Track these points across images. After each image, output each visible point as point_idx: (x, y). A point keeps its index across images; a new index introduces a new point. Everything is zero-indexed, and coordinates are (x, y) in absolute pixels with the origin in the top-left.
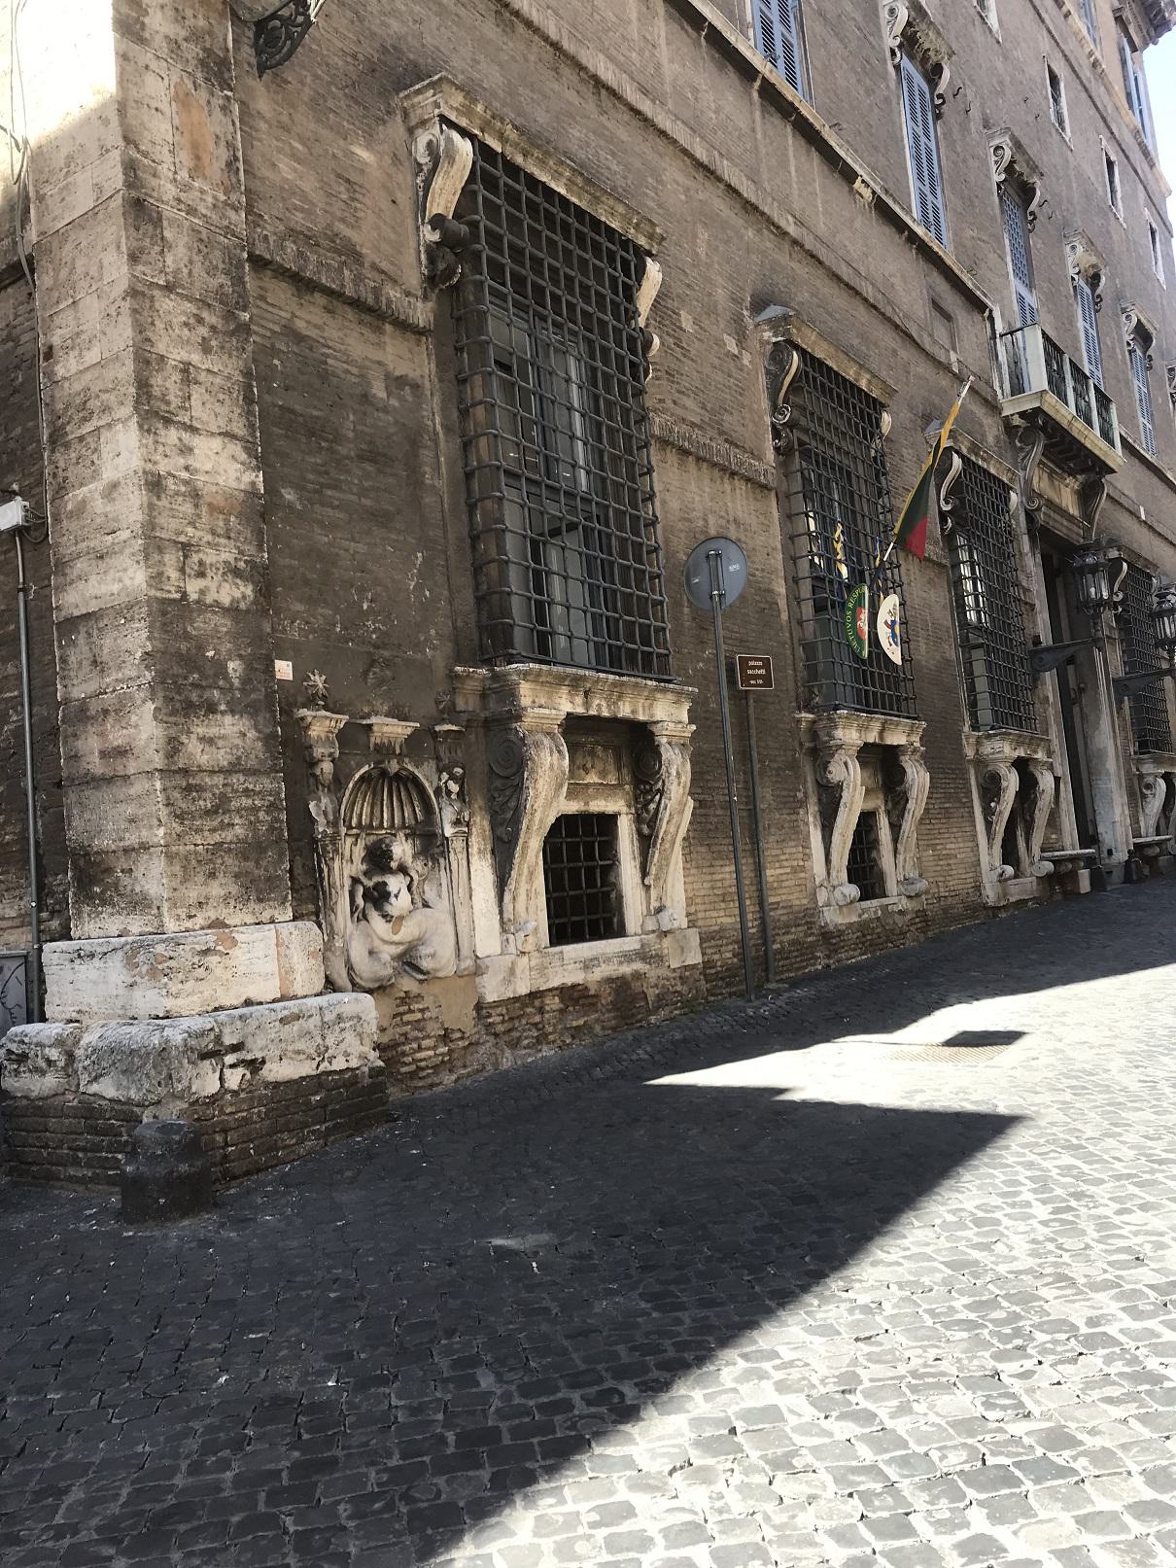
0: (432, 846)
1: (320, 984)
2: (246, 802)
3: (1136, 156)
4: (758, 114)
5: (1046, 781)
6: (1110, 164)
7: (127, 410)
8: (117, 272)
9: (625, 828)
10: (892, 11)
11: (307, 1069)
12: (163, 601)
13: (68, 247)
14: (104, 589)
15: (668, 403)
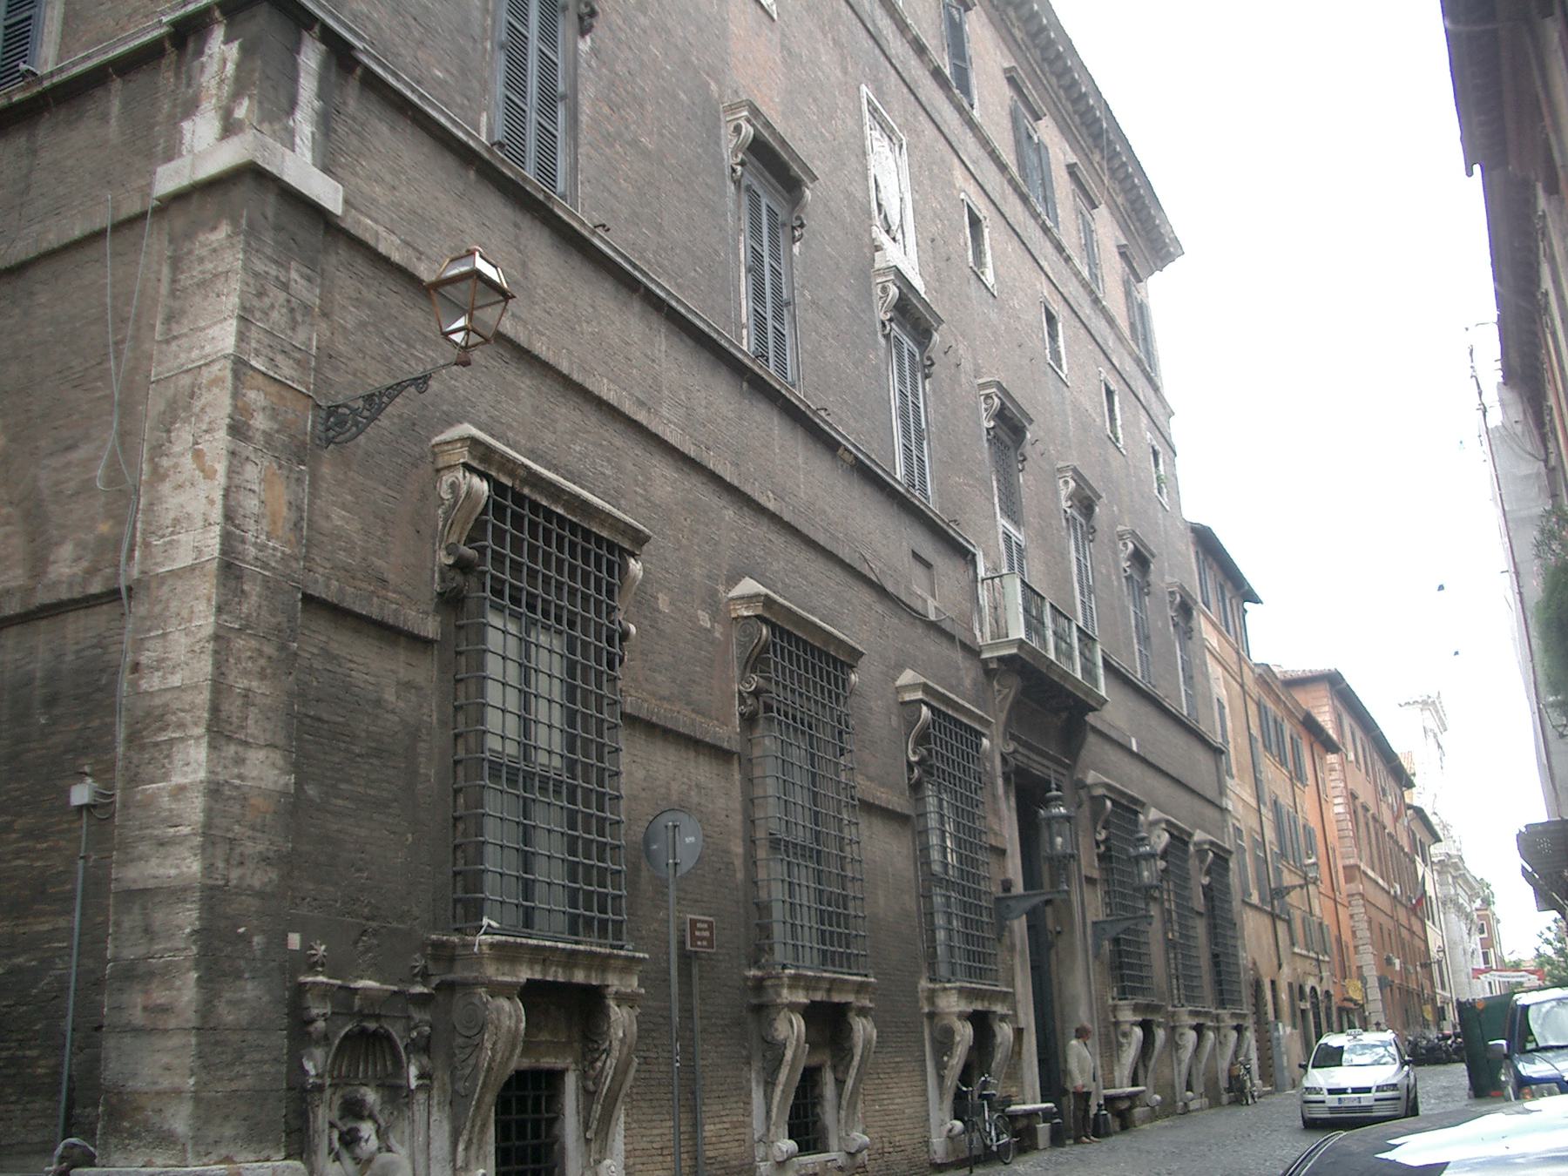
0: (396, 1095)
2: (257, 1056)
3: (1140, 384)
5: (1004, 1032)
6: (1110, 394)
7: (200, 730)
8: (205, 622)
9: (571, 1082)
12: (212, 888)
13: (165, 588)
14: (161, 871)
15: (638, 688)
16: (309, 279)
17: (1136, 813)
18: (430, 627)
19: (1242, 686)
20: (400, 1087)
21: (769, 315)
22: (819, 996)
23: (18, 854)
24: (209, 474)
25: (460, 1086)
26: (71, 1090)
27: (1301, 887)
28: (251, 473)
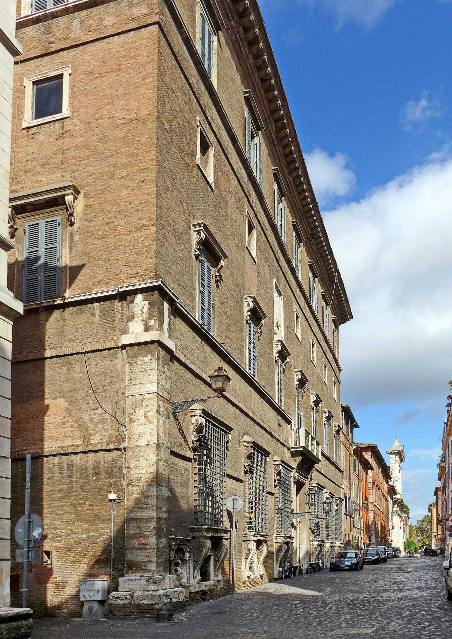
10: (277, 347)
20: (184, 560)
23: (88, 510)
26: (113, 562)
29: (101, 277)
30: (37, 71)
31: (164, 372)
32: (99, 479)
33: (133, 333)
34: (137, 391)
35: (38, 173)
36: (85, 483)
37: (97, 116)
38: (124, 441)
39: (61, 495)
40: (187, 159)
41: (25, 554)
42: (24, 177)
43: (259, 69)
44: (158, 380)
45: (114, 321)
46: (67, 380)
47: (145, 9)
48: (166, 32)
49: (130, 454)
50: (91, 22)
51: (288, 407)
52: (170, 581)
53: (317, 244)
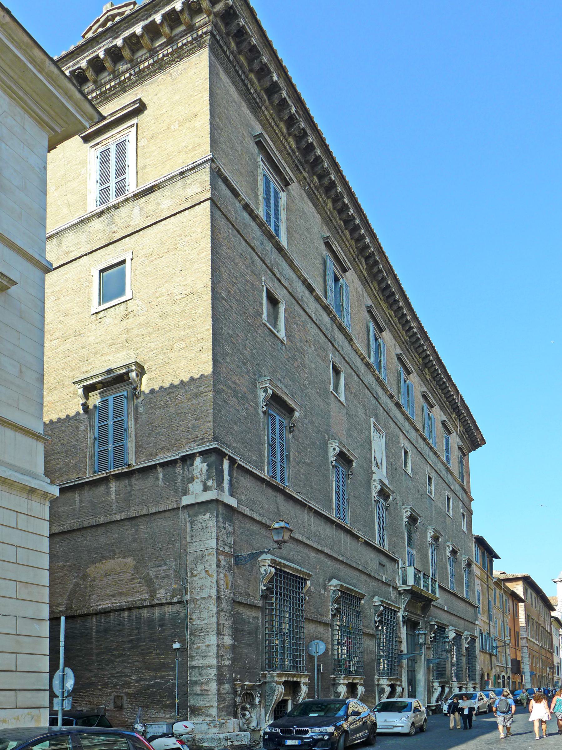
1: (238, 730)
4: (334, 531)
7: (214, 633)
8: (213, 609)
9: (290, 702)
10: (375, 486)
11: (240, 743)
16: (230, 525)
17: (445, 628)
18: (260, 604)
19: (488, 585)
21: (341, 504)
22: (350, 681)
23: (155, 658)
24: (211, 576)
25: (267, 704)
26: (178, 707)
27: (503, 646)
28: (222, 575)
29: (163, 444)
30: (103, 260)
31: (225, 528)
32: (164, 630)
33: (193, 493)
34: (198, 547)
35: (107, 354)
36: (152, 634)
37: (157, 295)
38: (186, 594)
39: (130, 645)
40: (250, 321)
41: (60, 702)
42: (93, 359)
43: (340, 212)
44: (217, 536)
45: (176, 483)
46: (135, 540)
47: (198, 187)
48: (219, 206)
49: (192, 606)
50: (149, 208)
51: (393, 546)
52: (233, 725)
53: (432, 373)
